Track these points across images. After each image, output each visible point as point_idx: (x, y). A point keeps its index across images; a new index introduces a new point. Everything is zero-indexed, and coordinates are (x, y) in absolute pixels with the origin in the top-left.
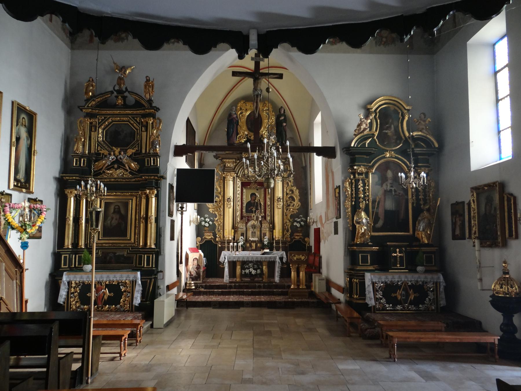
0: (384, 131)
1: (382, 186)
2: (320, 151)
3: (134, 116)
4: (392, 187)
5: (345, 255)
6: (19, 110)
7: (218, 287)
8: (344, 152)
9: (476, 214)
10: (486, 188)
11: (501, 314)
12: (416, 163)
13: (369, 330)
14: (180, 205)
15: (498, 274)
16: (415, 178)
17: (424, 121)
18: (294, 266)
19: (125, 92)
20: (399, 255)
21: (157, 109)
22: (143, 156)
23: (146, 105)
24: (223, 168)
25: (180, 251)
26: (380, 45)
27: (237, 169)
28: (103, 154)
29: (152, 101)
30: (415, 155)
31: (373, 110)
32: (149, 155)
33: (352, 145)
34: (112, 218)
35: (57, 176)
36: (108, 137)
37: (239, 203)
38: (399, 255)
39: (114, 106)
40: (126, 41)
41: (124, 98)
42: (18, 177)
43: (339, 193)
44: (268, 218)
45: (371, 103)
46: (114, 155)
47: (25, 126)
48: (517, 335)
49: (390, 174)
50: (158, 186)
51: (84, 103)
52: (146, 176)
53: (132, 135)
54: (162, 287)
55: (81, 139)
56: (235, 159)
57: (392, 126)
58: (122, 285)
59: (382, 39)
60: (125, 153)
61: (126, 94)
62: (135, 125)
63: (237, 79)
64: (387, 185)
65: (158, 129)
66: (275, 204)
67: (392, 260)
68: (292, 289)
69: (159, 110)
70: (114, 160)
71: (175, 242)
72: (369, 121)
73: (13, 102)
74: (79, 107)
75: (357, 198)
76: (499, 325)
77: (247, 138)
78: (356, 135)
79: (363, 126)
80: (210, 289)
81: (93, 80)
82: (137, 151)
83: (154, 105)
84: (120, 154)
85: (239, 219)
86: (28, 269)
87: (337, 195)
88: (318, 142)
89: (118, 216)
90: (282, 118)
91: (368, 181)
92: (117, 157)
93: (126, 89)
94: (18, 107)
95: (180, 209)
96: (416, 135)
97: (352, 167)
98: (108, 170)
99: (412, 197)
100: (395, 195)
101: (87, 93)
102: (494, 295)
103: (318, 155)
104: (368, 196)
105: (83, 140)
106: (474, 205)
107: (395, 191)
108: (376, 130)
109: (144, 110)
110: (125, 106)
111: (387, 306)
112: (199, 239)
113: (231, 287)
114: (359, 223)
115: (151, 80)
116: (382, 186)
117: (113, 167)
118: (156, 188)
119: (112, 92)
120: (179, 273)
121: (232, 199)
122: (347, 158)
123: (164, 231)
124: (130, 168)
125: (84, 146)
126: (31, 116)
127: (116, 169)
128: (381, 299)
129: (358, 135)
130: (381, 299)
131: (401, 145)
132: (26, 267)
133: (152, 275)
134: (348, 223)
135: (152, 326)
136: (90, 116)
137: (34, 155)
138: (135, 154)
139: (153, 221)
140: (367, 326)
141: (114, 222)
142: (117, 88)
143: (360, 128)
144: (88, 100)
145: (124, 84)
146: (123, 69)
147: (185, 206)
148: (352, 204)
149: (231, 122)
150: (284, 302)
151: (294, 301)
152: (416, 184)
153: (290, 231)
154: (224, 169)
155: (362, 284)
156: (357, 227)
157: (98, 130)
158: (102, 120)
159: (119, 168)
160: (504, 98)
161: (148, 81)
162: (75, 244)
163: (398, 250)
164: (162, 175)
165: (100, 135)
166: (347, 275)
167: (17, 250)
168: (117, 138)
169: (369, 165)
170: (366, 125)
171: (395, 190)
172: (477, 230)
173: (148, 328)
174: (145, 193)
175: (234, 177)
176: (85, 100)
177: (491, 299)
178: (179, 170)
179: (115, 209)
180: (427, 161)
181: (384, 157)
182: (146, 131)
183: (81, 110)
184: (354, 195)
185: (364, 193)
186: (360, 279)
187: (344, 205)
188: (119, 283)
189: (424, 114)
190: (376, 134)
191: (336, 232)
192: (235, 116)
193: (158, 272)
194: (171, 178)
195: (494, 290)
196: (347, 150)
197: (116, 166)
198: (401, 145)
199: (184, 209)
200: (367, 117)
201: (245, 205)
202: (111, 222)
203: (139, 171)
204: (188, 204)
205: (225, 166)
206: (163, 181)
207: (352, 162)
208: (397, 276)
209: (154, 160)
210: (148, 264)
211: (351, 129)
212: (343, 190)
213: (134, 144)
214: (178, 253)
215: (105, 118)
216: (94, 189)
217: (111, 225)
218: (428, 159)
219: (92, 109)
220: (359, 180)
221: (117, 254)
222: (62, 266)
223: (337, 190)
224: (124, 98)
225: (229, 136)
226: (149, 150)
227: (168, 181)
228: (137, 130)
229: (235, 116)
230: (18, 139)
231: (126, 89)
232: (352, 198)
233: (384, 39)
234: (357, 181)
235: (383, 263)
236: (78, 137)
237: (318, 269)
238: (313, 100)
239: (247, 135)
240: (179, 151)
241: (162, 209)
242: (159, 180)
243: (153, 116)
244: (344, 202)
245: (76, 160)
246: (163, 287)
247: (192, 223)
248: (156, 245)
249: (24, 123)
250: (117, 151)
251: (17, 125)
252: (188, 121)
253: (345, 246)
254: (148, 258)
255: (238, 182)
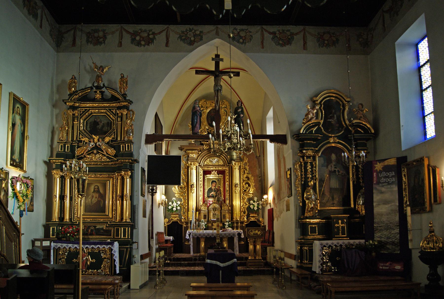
0: (328, 120)
1: (327, 167)
2: (273, 139)
3: (110, 109)
4: (336, 168)
5: (296, 227)
6: (16, 100)
7: (185, 259)
8: (294, 138)
9: (407, 187)
10: (415, 163)
11: (427, 266)
12: (357, 146)
13: (317, 287)
14: (151, 188)
15: (426, 233)
16: (356, 156)
17: (362, 111)
18: (251, 241)
19: (103, 87)
20: (342, 225)
21: (131, 102)
22: (119, 143)
23: (121, 98)
24: (187, 159)
25: (151, 229)
26: (322, 47)
27: (199, 160)
28: (84, 141)
29: (126, 95)
30: (355, 140)
31: (318, 102)
32: (124, 142)
33: (301, 132)
34: (93, 197)
35: (47, 160)
36: (88, 126)
37: (202, 189)
38: (342, 225)
39: (94, 100)
40: (103, 44)
41: (102, 93)
42: (14, 157)
43: (290, 175)
44: (228, 202)
45: (316, 96)
46: (94, 142)
47: (19, 114)
48: (441, 283)
49: (333, 157)
50: (132, 169)
51: (68, 97)
52: (122, 159)
53: (109, 124)
54: (136, 256)
55: (65, 128)
56: (198, 150)
57: (335, 116)
58: (103, 253)
59: (324, 42)
60: (103, 139)
61: (104, 90)
62: (111, 116)
63: (201, 77)
64: (332, 167)
65: (132, 119)
66: (234, 189)
67: (336, 230)
68: (250, 260)
69: (132, 103)
70: (94, 146)
71: (147, 219)
72: (315, 111)
73: (10, 93)
74: (63, 101)
75: (306, 178)
76: (426, 277)
77: (208, 132)
78: (304, 124)
79: (310, 116)
80: (178, 262)
81: (75, 77)
82: (113, 138)
83: (127, 98)
84: (99, 141)
85: (201, 203)
86: (23, 234)
87: (288, 176)
88: (270, 131)
89: (97, 195)
90: (240, 110)
91: (315, 163)
92: (96, 144)
93: (104, 85)
94: (14, 98)
95: (150, 191)
96: (356, 123)
97: (301, 151)
98: (88, 154)
99: (353, 176)
100: (339, 175)
101: (70, 89)
102: (422, 250)
103: (271, 141)
104: (315, 176)
105: (67, 129)
106: (405, 179)
107: (339, 172)
108: (321, 119)
109: (119, 102)
110: (103, 100)
111: (333, 268)
112: (167, 220)
113: (195, 260)
114: (308, 199)
115: (125, 77)
116: (327, 167)
117: (93, 153)
118: (130, 170)
119: (91, 88)
120: (150, 247)
121: (195, 186)
122: (297, 144)
123: (138, 208)
124: (107, 153)
125: (67, 134)
126: (24, 106)
127: (95, 154)
128: (328, 262)
129: (306, 123)
130: (328, 262)
131: (342, 132)
132: (22, 231)
133: (127, 245)
134: (299, 199)
135: (129, 286)
136: (73, 108)
137: (26, 139)
138: (112, 141)
139: (128, 198)
140: (315, 284)
141: (95, 200)
142: (96, 84)
143: (308, 117)
144: (70, 95)
145: (102, 81)
146: (102, 68)
147: (155, 188)
148: (302, 184)
149: (195, 113)
150: (243, 270)
151: (252, 270)
152: (356, 162)
153: (246, 213)
154: (188, 159)
155: (311, 251)
156: (307, 203)
157: (80, 120)
158: (83, 112)
159: (98, 153)
160: (427, 88)
161: (122, 77)
162: (62, 218)
163: (340, 221)
164: (135, 158)
165: (81, 124)
166: (298, 244)
167: (16, 218)
168: (95, 128)
169: (316, 149)
170: (313, 114)
171: (338, 170)
172: (408, 199)
173: (125, 288)
174: (121, 175)
175: (197, 166)
176: (69, 95)
177: (420, 254)
178: (149, 156)
179: (94, 188)
180: (365, 145)
181: (329, 143)
182: (122, 121)
183: (65, 103)
184: (303, 176)
185: (312, 174)
186: (309, 247)
187: (295, 184)
188: (99, 251)
189: (362, 104)
190: (322, 122)
191: (288, 209)
192: (198, 109)
193: (133, 243)
194: (143, 163)
195: (422, 246)
196: (297, 136)
197: (95, 151)
198: (342, 132)
199: (154, 191)
200: (313, 108)
201: (206, 191)
202: (91, 200)
203: (115, 156)
204: (158, 186)
205: (188, 156)
206: (136, 164)
207: (302, 147)
208: (342, 241)
209: (128, 146)
210: (124, 235)
211: (299, 118)
212: (294, 172)
213: (111, 133)
214: (149, 230)
215: (86, 110)
216: (78, 169)
217: (91, 203)
218: (366, 144)
219: (75, 102)
220: (307, 162)
221: (97, 227)
222: (51, 237)
223: (289, 173)
224: (102, 93)
225: (193, 127)
226: (124, 138)
227: (141, 165)
228: (113, 120)
229: (198, 109)
230: (14, 125)
231: (104, 85)
232: (302, 178)
233: (326, 42)
234: (306, 163)
235: (327, 231)
236: (63, 126)
237: (272, 243)
238: (266, 93)
239: (208, 129)
240: (149, 139)
241: (135, 188)
242: (133, 163)
243: (127, 108)
244: (295, 182)
245: (61, 146)
246: (137, 257)
247: (161, 205)
248: (131, 219)
249: (18, 112)
250: (96, 138)
251: (13, 113)
252: (156, 115)
253: (296, 220)
254: (125, 230)
255: (200, 171)
